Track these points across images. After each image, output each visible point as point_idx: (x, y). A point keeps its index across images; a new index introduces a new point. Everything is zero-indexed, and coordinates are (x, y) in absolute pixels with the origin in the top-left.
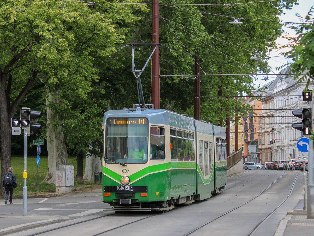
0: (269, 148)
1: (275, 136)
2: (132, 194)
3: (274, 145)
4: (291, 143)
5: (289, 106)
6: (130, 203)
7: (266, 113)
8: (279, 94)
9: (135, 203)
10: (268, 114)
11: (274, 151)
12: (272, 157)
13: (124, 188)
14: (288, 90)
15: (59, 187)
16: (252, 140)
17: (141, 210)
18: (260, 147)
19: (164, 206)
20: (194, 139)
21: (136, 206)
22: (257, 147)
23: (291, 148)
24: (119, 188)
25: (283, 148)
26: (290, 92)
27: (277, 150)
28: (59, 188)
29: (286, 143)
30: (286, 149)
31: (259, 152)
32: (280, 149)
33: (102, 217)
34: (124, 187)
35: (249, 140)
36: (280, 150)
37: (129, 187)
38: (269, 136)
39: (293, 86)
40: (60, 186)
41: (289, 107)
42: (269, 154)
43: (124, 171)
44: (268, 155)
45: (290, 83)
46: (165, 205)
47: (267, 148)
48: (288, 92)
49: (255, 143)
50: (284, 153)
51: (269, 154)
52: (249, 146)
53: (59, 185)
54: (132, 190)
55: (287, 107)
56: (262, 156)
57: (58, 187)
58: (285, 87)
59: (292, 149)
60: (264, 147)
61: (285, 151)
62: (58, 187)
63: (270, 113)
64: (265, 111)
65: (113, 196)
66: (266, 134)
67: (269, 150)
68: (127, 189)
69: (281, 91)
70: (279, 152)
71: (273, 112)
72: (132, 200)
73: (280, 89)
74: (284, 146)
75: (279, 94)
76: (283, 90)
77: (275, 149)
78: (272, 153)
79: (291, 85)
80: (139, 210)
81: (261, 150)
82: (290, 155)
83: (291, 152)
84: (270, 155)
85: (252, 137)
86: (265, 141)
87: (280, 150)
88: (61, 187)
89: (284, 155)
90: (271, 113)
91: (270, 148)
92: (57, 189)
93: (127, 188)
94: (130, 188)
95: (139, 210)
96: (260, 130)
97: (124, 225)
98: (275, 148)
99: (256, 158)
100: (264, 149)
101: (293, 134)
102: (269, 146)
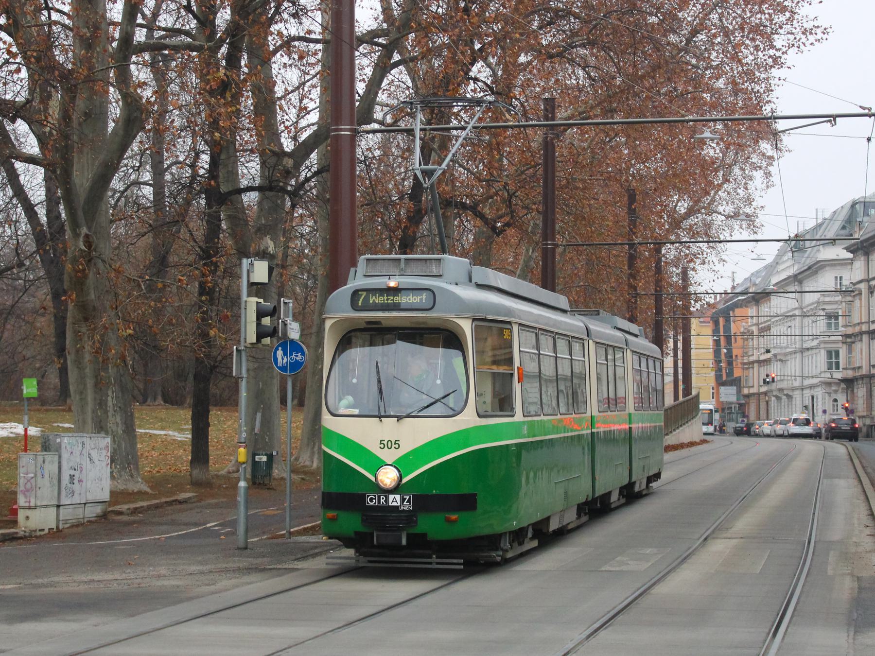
0: (762, 393)
1: (775, 370)
2: (409, 518)
3: (774, 386)
4: (807, 382)
5: (802, 309)
6: (404, 542)
7: (757, 324)
8: (782, 289)
9: (419, 543)
10: (760, 326)
11: (773, 399)
12: (770, 411)
13: (386, 501)
14: (800, 277)
15: (30, 508)
16: (729, 379)
17: (438, 563)
18: (745, 391)
19: (502, 545)
20: (584, 356)
21: (421, 551)
22: (739, 391)
23: (807, 393)
24: (371, 500)
25: (790, 393)
26: (805, 282)
27: (778, 398)
28: (29, 513)
29: (797, 384)
30: (797, 394)
31: (743, 402)
32: (785, 395)
33: (81, 653)
34: (386, 497)
35: (724, 378)
36: (785, 397)
37: (398, 497)
38: (762, 369)
39: (809, 268)
40: (32, 504)
41: (803, 312)
42: (763, 405)
43: (394, 446)
44: (761, 407)
45: (804, 263)
46: (505, 543)
47: (759, 394)
48: (800, 282)
49: (736, 382)
50: (794, 403)
51: (763, 405)
52: (722, 389)
53: (30, 502)
54: (407, 506)
55: (797, 312)
56: (749, 409)
57: (24, 508)
58: (791, 272)
59: (809, 395)
60: (752, 391)
61: (794, 400)
62: (24, 508)
63: (763, 325)
64: (755, 320)
65: (351, 522)
66: (756, 365)
67: (762, 397)
68: (395, 504)
69: (785, 279)
70: (783, 401)
71: (769, 323)
72: (409, 536)
73: (783, 276)
74: (793, 389)
75: (782, 289)
76: (789, 277)
77: (774, 396)
78: (770, 403)
79: (806, 267)
80: (430, 563)
81: (748, 396)
82: (805, 407)
83: (807, 402)
84: (765, 406)
85: (730, 373)
86: (754, 382)
87: (784, 397)
88: (35, 507)
89: (794, 406)
90: (767, 324)
91: (765, 393)
92: (21, 515)
93: (394, 500)
94: (403, 500)
95: (430, 563)
96: (745, 358)
97: (417, 594)
98: (775, 393)
99: (737, 413)
100: (754, 394)
101: (810, 364)
102: (764, 389)
